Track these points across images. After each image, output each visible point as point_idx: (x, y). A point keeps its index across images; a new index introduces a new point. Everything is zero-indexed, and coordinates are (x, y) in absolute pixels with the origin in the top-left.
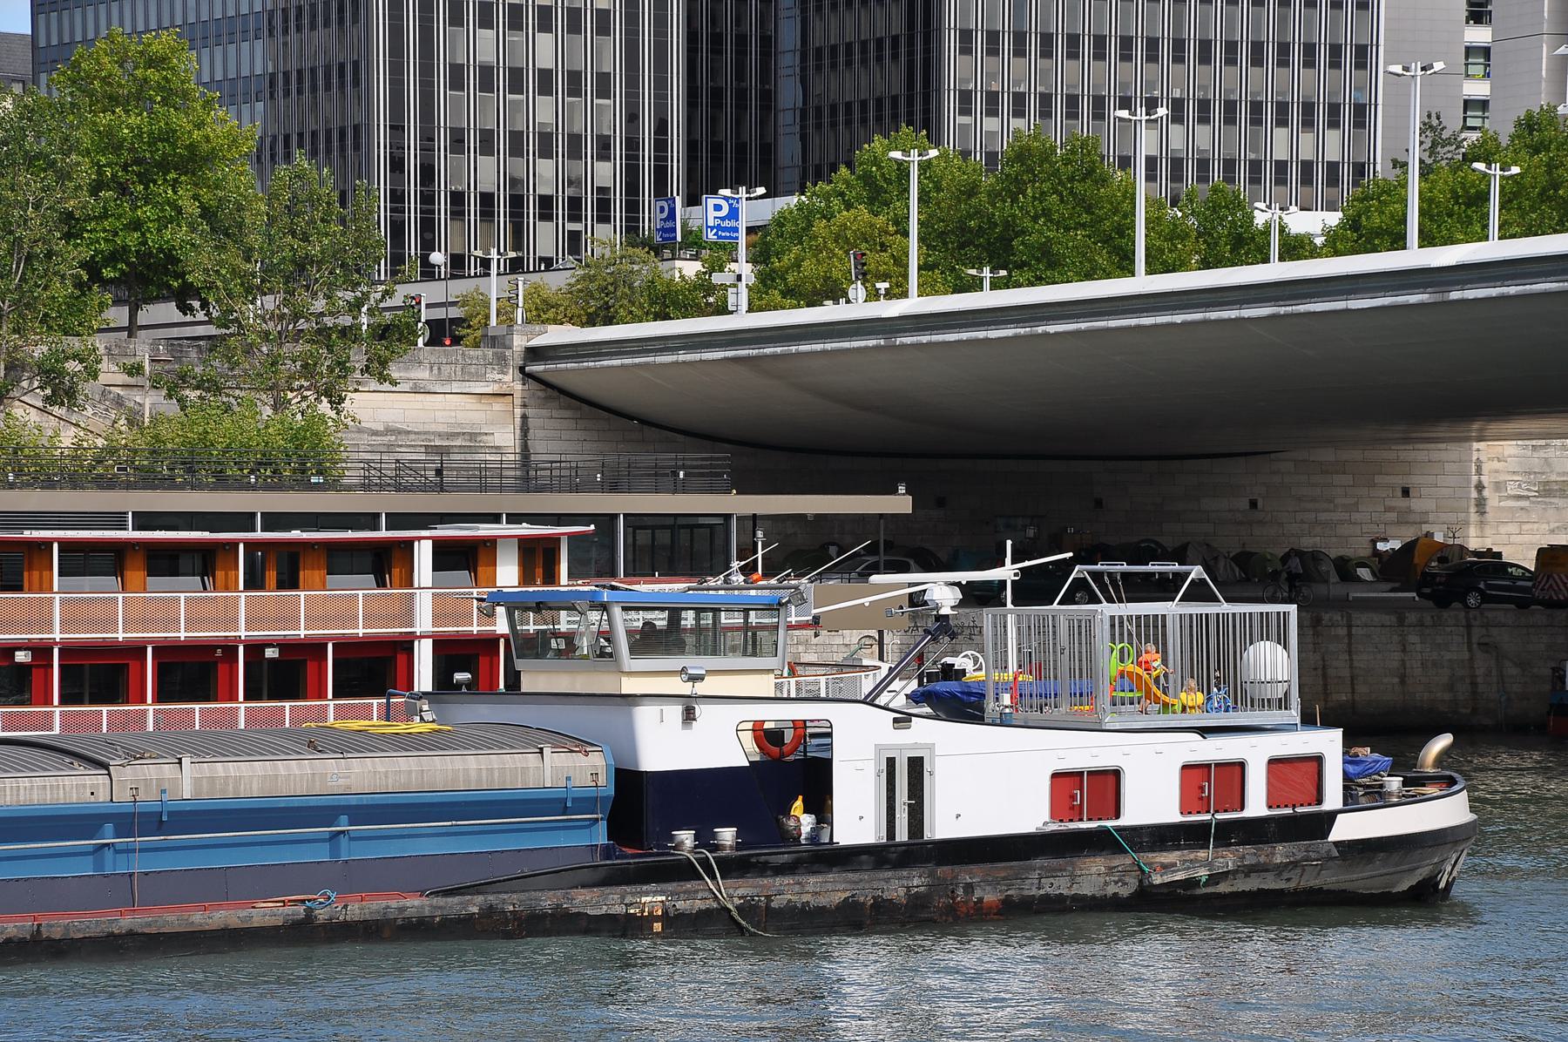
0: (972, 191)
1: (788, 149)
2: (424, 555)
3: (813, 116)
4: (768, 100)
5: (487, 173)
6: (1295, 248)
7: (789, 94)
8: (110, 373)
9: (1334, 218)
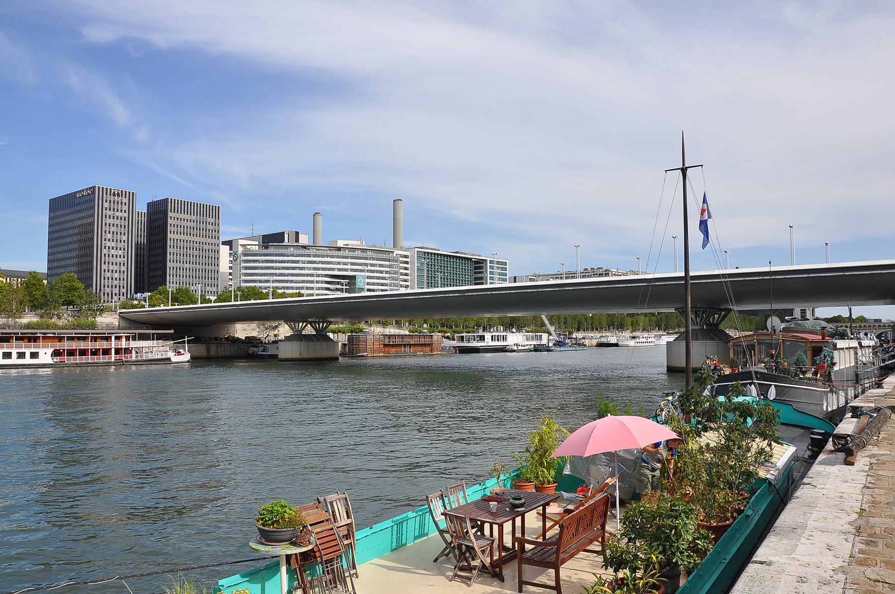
2: (113, 338)
8: (65, 315)
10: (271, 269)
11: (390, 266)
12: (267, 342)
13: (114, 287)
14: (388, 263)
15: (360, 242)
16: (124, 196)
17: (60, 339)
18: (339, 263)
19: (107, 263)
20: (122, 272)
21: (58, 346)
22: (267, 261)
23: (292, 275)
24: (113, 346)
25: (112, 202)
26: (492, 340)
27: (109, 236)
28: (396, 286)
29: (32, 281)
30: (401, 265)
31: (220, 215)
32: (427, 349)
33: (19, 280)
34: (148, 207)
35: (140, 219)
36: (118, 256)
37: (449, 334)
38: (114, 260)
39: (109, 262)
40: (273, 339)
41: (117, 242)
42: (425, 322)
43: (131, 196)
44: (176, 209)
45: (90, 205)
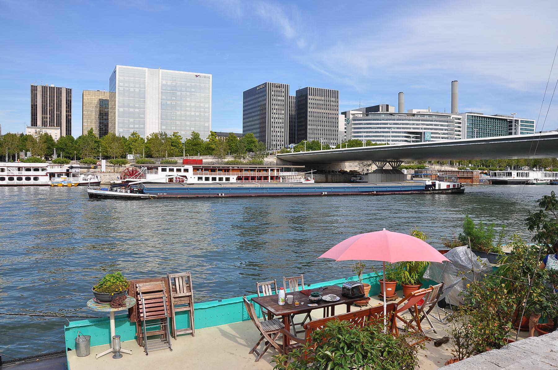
0: (310, 144)
1: (296, 141)
2: (269, 170)
3: (298, 139)
4: (295, 138)
5: (274, 143)
6: (333, 149)
7: (296, 137)
8: (248, 157)
9: (336, 147)
10: (370, 129)
11: (448, 126)
12: (362, 174)
13: (278, 141)
14: (446, 124)
15: (428, 110)
16: (282, 87)
17: (241, 170)
18: (413, 124)
19: (273, 127)
20: (282, 132)
21: (240, 174)
22: (368, 124)
23: (383, 132)
24: (269, 175)
25: (276, 91)
26: (517, 176)
27: (275, 111)
28: (452, 139)
29: (231, 137)
30: (456, 125)
31: (339, 96)
32: (469, 180)
33: (225, 137)
34: (296, 93)
35: (292, 100)
36: (280, 123)
37: (486, 171)
38: (278, 125)
39: (274, 127)
40: (365, 172)
41: (279, 114)
42: (470, 163)
43: (287, 87)
44: (312, 93)
45: (264, 94)
